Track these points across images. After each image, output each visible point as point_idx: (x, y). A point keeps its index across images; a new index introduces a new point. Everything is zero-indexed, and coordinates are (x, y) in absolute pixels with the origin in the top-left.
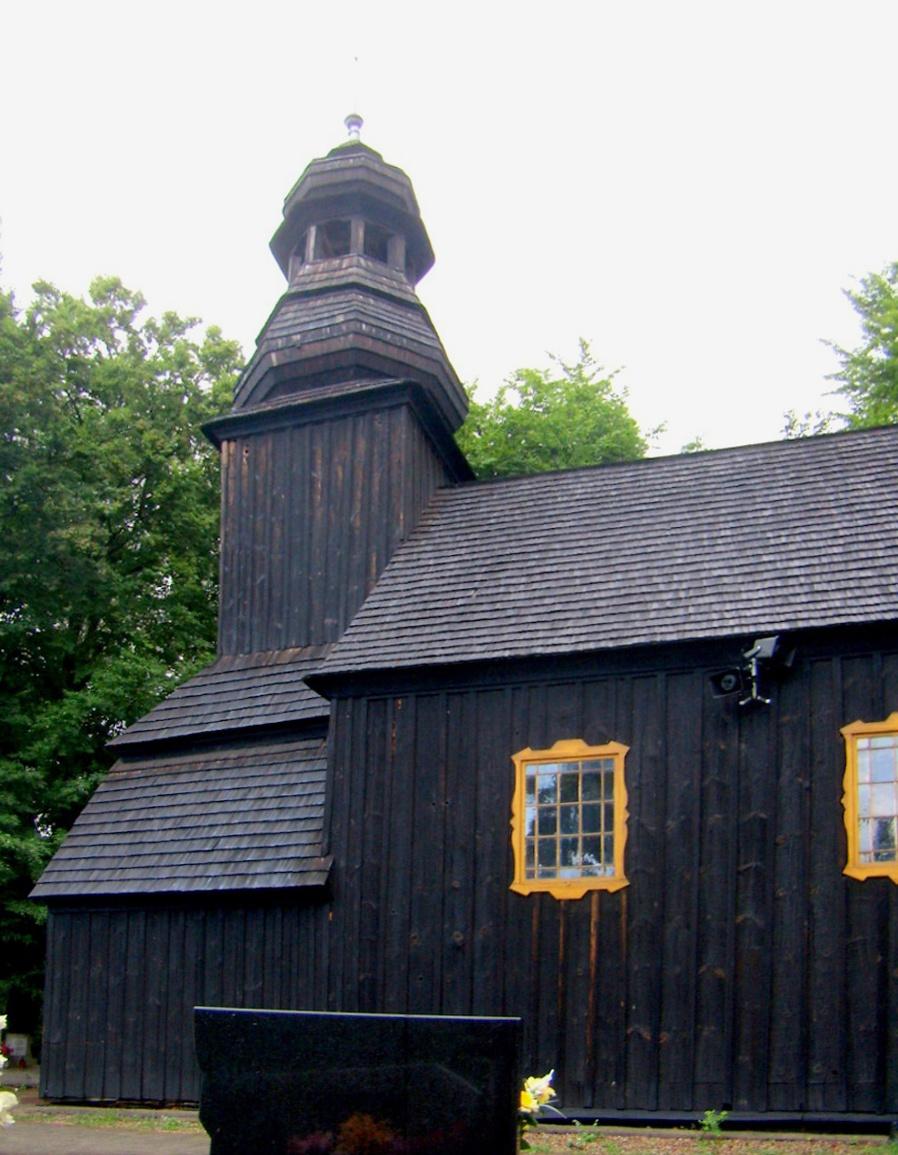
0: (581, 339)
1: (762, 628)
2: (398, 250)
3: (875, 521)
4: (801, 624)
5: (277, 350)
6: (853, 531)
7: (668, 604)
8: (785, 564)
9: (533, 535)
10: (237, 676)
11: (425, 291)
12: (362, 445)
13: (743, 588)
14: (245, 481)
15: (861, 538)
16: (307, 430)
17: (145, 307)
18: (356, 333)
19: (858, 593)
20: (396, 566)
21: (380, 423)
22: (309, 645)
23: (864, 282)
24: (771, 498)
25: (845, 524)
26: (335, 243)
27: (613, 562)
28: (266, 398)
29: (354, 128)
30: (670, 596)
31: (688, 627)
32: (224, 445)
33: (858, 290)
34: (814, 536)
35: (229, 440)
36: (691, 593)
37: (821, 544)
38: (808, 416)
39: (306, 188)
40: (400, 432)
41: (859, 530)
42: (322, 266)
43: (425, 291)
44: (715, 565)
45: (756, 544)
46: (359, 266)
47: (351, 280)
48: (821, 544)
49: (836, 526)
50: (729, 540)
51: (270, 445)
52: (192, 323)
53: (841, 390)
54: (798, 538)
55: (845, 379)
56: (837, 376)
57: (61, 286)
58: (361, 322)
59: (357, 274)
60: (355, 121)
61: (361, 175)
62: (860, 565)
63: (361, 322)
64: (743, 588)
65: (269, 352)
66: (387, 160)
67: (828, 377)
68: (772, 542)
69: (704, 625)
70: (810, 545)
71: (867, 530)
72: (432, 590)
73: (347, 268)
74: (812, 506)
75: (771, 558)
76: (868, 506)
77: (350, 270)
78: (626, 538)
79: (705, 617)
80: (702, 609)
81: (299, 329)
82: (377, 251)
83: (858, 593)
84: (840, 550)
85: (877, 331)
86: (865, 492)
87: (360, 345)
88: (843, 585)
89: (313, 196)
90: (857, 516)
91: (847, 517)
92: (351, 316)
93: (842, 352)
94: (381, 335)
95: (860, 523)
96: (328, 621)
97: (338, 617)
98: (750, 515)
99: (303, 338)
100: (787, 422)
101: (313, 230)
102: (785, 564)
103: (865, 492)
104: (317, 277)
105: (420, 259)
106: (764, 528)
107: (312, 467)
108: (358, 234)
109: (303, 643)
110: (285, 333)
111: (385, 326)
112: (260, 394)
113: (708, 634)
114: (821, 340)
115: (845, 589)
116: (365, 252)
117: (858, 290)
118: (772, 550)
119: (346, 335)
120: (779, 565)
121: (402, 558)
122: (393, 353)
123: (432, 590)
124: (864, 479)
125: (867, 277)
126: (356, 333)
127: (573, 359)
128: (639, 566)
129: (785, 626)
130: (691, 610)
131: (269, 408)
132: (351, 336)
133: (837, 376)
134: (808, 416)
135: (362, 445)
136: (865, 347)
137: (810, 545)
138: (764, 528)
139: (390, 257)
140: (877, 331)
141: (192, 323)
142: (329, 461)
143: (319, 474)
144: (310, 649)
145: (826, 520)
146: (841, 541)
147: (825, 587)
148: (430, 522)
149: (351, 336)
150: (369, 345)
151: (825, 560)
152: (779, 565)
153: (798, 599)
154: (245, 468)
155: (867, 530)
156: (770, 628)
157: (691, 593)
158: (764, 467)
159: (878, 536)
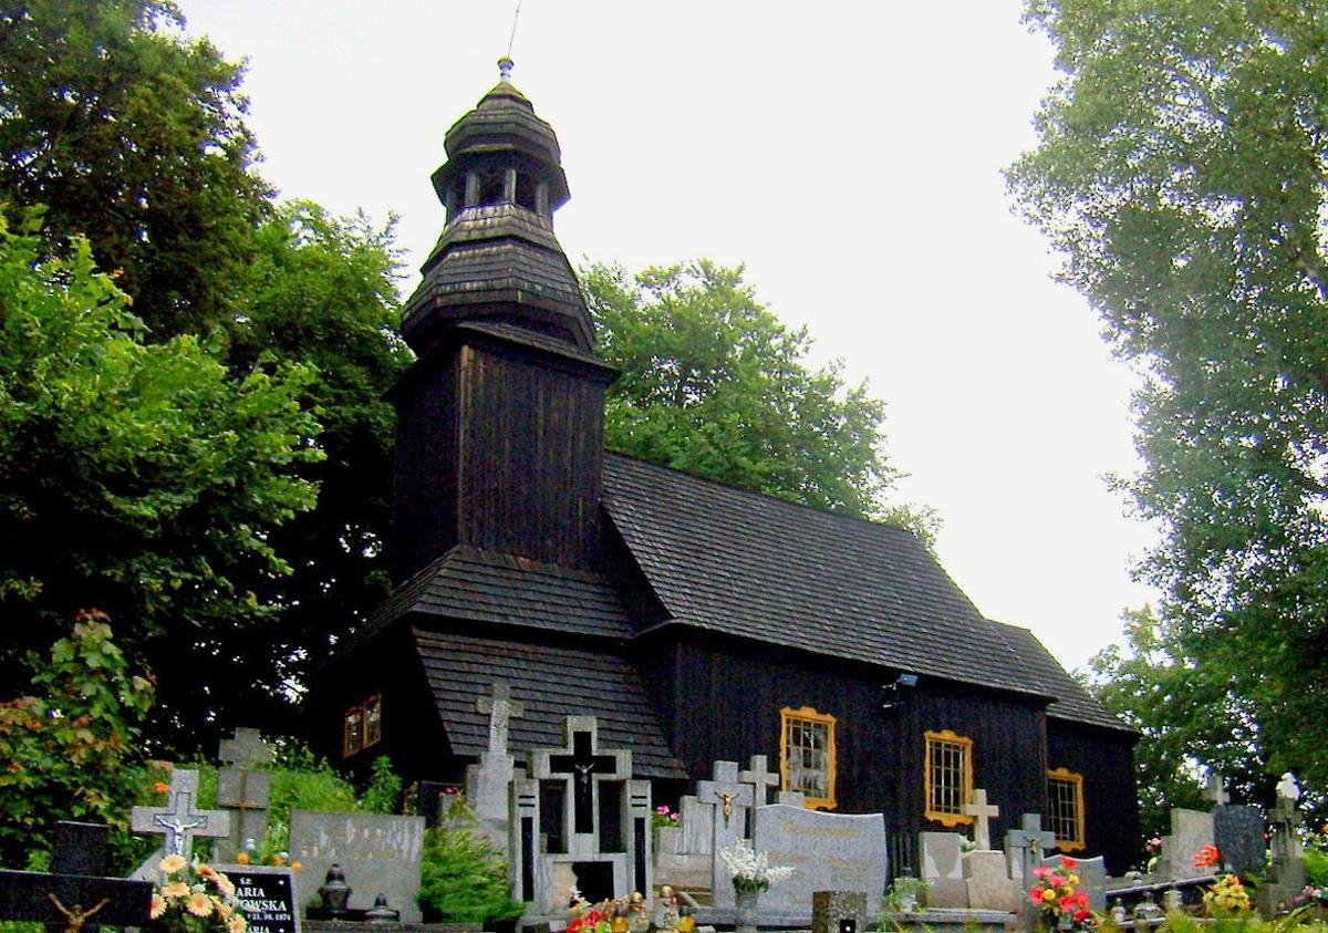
26: (490, 196)
35: (471, 346)
81: (543, 282)
82: (525, 199)
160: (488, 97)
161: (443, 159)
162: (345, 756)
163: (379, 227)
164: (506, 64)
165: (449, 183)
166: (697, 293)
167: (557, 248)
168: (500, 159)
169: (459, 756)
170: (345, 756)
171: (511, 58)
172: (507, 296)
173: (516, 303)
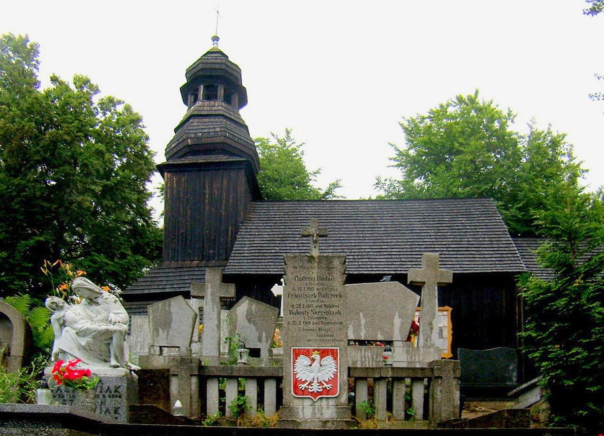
0: (286, 129)
1: (386, 272)
2: (235, 98)
3: (420, 237)
4: (399, 272)
5: (191, 138)
6: (413, 240)
7: (352, 260)
8: (391, 250)
9: (295, 227)
10: (173, 270)
11: (245, 114)
12: (225, 182)
13: (377, 257)
14: (175, 191)
15: (416, 243)
16: (202, 173)
17: (99, 94)
18: (224, 137)
19: (416, 263)
20: (242, 233)
21: (233, 174)
22: (203, 260)
23: (408, 121)
24: (383, 223)
25: (410, 237)
26: (210, 96)
27: (328, 242)
28: (181, 157)
29: (215, 42)
30: (352, 257)
31: (360, 269)
32: (166, 174)
33: (406, 124)
34: (400, 240)
35: (168, 172)
36: (359, 257)
37: (403, 244)
38: (386, 180)
39: (198, 69)
40: (242, 178)
41: (416, 240)
42: (207, 103)
43: (245, 114)
44: (366, 247)
45: (379, 241)
46: (222, 106)
47: (221, 113)
48: (403, 244)
49: (407, 237)
50: (370, 238)
51: (186, 176)
52: (119, 102)
53: (398, 166)
54: (395, 241)
55: (398, 161)
56: (395, 159)
57: (62, 78)
58: (227, 132)
59: (222, 110)
60: (216, 39)
61: (223, 67)
62: (416, 253)
63: (227, 132)
64: (377, 257)
65: (187, 139)
66: (230, 59)
67: (390, 159)
68: (385, 241)
69: (366, 269)
70: (399, 244)
71: (418, 240)
72: (261, 245)
73: (217, 106)
74: (398, 229)
75: (386, 247)
76: (418, 231)
77: (219, 108)
78: (332, 233)
79: (366, 266)
80: (364, 263)
81: (200, 131)
82: (227, 99)
83: (416, 263)
84: (409, 247)
85: (412, 141)
86: (416, 226)
87: (226, 142)
88: (411, 260)
89: (201, 73)
90: (414, 235)
91: (411, 234)
92: (223, 129)
93: (398, 150)
94: (234, 138)
95: (415, 237)
96: (211, 251)
97: (215, 250)
98: (376, 229)
99: (202, 135)
100: (377, 181)
101: (202, 87)
102: (391, 250)
103: (416, 226)
104: (205, 108)
105: (243, 101)
106: (382, 235)
107: (205, 188)
108: (221, 92)
109: (200, 259)
110: (194, 132)
111: (235, 134)
112: (180, 154)
113: (368, 272)
114: (390, 144)
115: (412, 261)
116: (224, 100)
117: (406, 124)
118: (386, 244)
119: (220, 136)
120: (389, 250)
121: (243, 230)
122: (239, 147)
123: (261, 245)
124: (416, 220)
125: (410, 119)
126: (224, 137)
127: (282, 136)
128: (338, 245)
129: (393, 272)
130: (360, 263)
131: (187, 162)
132: (222, 138)
133: (395, 159)
134: (386, 180)
135: (225, 182)
136: (407, 149)
137: (399, 244)
138: (382, 235)
139: (232, 102)
140: (412, 141)
141: (119, 102)
142: (211, 187)
143: (207, 191)
144: (203, 262)
145: (403, 235)
146: (409, 243)
147: (405, 260)
148: (251, 216)
149: (222, 138)
150: (229, 142)
151: (404, 250)
152: (389, 250)
153: (396, 263)
154: (175, 185)
155: (418, 240)
156: (388, 272)
157: (359, 257)
158: (379, 210)
159: (422, 243)
160: (209, 53)
161: (184, 81)
162: (181, 406)
163: (282, 136)
164: (216, 39)
165: (188, 92)
166: (38, 88)
167: (241, 122)
168: (214, 81)
169: (453, 279)
170: (181, 406)
171: (218, 36)
172: (185, 144)
173: (188, 145)
